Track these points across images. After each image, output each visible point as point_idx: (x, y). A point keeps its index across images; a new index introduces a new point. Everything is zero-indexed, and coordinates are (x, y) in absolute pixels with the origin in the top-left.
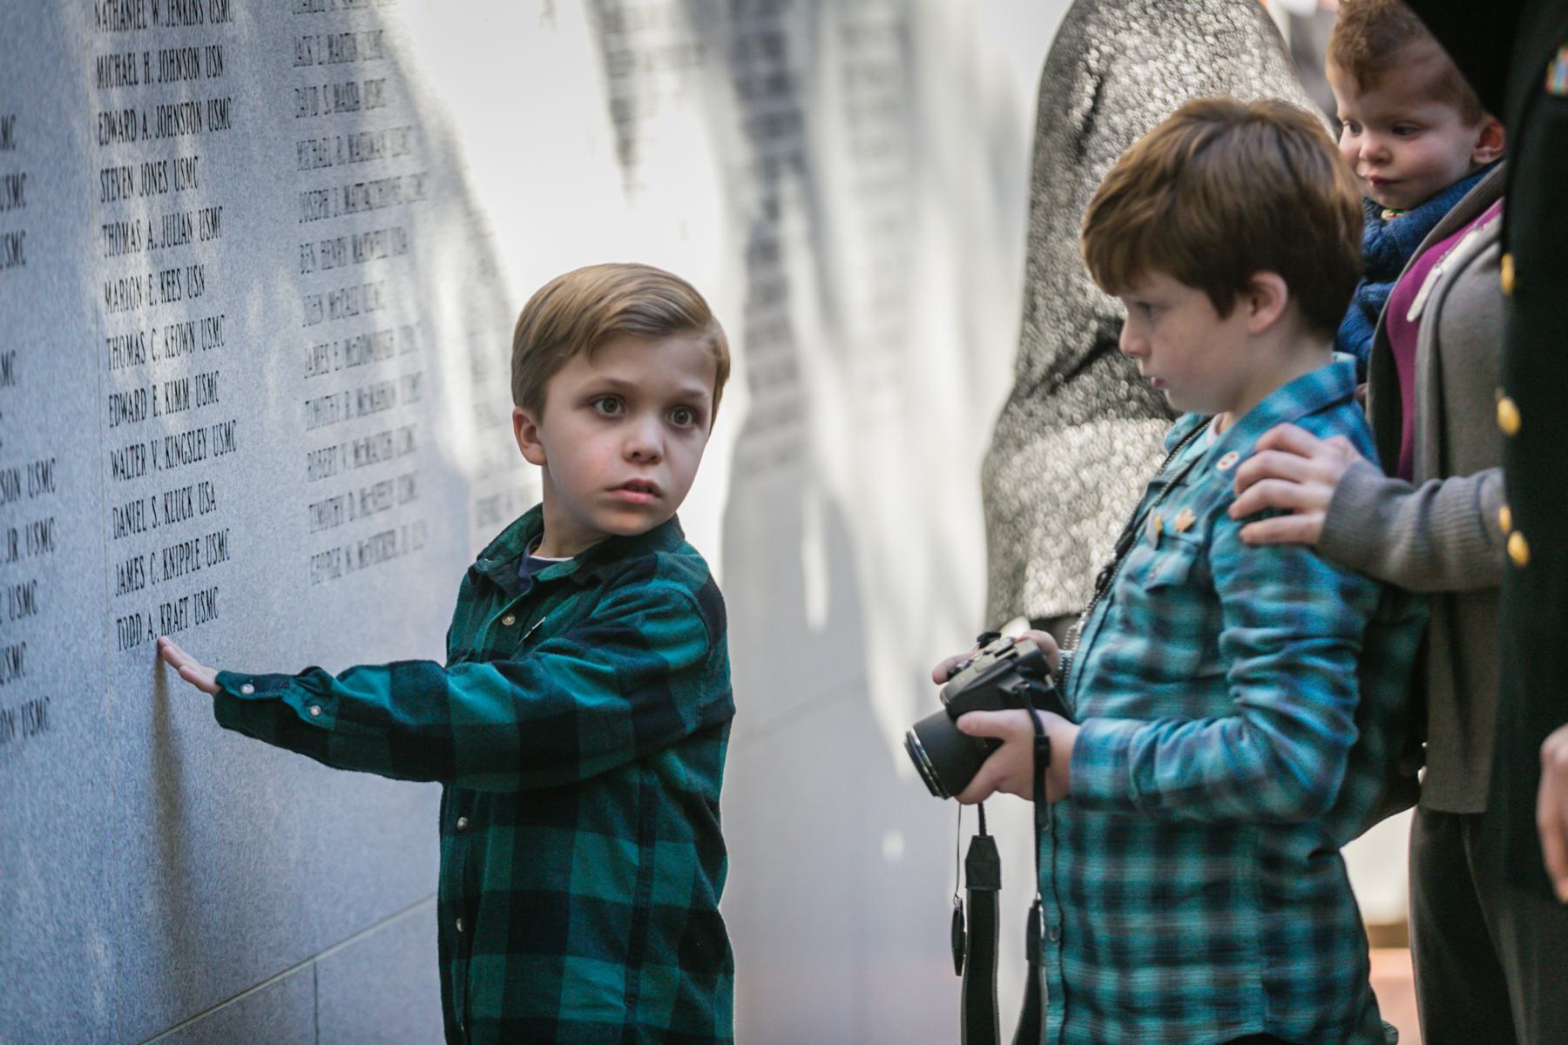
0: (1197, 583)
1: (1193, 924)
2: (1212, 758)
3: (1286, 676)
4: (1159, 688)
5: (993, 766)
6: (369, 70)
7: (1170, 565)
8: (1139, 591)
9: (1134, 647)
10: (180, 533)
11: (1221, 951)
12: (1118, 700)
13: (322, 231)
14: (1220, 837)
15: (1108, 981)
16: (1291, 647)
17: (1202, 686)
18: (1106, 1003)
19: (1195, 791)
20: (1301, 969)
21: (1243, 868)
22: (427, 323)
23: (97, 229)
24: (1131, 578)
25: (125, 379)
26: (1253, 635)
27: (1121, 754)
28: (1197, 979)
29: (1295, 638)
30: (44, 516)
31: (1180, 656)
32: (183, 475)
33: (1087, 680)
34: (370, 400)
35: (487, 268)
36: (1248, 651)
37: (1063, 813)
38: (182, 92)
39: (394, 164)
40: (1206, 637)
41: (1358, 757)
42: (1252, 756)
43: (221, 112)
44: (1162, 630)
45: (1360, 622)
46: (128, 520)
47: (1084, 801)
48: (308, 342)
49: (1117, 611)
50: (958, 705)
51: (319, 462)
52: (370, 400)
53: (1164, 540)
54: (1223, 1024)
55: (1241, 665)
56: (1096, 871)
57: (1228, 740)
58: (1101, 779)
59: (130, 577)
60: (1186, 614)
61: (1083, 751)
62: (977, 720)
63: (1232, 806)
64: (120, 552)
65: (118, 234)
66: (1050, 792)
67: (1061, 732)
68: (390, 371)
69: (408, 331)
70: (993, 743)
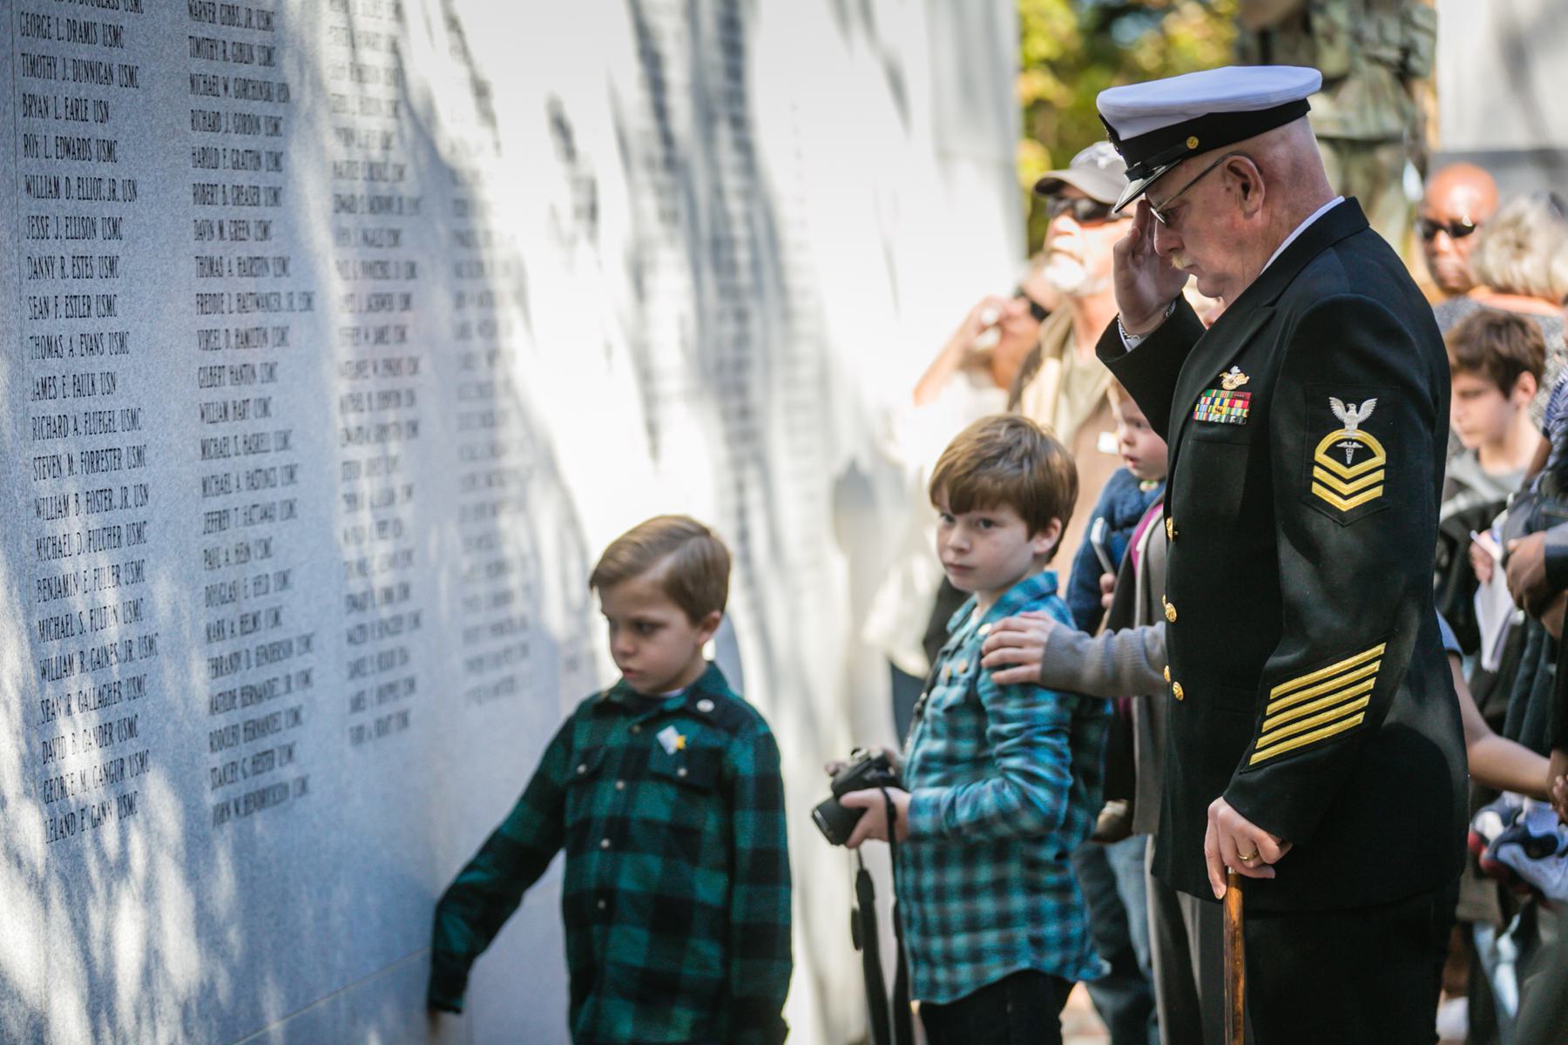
0: (971, 703)
1: (987, 906)
2: (988, 802)
3: (1026, 749)
4: (958, 768)
5: (864, 824)
6: (504, 403)
7: (954, 694)
8: (939, 712)
9: (938, 746)
10: (387, 678)
11: (1004, 921)
12: (934, 777)
13: (472, 499)
14: (1000, 851)
15: (937, 944)
16: (1028, 732)
17: (980, 764)
18: (937, 957)
19: (981, 823)
20: (1051, 930)
21: (1014, 870)
22: (536, 554)
23: (339, 497)
24: (935, 705)
25: (356, 586)
26: (1005, 728)
27: (936, 807)
28: (990, 938)
29: (1031, 727)
30: (306, 667)
31: (966, 747)
32: (389, 643)
33: (915, 768)
34: (502, 598)
35: (571, 520)
36: (1002, 738)
37: (907, 849)
38: (391, 416)
39: (513, 460)
40: (979, 734)
41: (1074, 794)
42: (1012, 798)
43: (414, 427)
44: (954, 733)
45: (1068, 716)
46: (357, 669)
47: (917, 837)
48: (465, 564)
49: (928, 727)
50: (839, 789)
51: (470, 635)
52: (502, 598)
53: (951, 681)
54: (1006, 964)
55: (1000, 746)
56: (929, 879)
57: (997, 790)
58: (925, 822)
59: (357, 704)
60: (967, 722)
61: (915, 807)
62: (853, 798)
63: (1003, 829)
64: (352, 688)
65: (352, 500)
66: (898, 834)
67: (901, 798)
68: (514, 581)
69: (523, 559)
70: (861, 811)
